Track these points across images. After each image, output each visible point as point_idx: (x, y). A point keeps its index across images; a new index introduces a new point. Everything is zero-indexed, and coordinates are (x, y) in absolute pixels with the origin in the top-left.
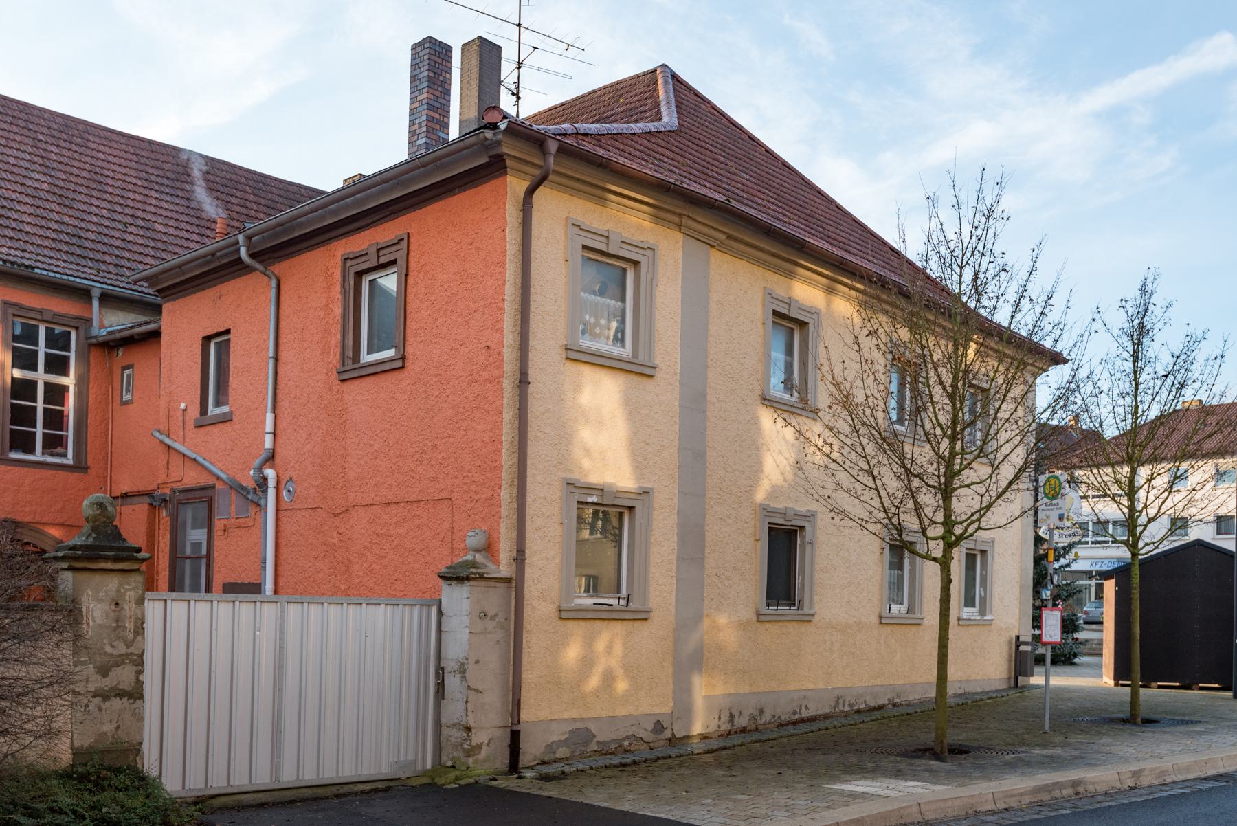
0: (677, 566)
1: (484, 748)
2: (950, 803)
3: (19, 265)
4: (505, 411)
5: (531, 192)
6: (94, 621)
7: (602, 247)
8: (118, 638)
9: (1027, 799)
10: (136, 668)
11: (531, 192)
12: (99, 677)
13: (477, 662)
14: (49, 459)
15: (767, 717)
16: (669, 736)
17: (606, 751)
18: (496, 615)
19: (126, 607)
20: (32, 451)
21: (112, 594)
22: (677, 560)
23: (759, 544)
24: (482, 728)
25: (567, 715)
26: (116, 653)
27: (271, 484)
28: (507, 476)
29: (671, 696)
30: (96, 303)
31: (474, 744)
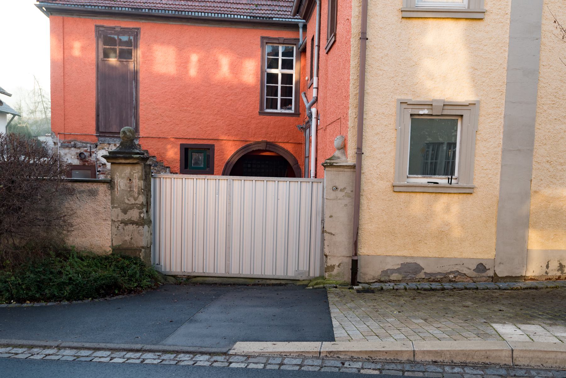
0: (503, 159)
1: (336, 268)
2: (553, 355)
3: (266, 18)
4: (352, 59)
6: (120, 187)
8: (131, 196)
10: (139, 211)
12: (123, 214)
13: (331, 217)
14: (283, 111)
17: (431, 278)
18: (345, 188)
19: (134, 181)
20: (277, 108)
21: (128, 175)
22: (503, 152)
24: (334, 256)
25: (399, 253)
26: (130, 203)
27: (314, 116)
28: (353, 101)
29: (494, 247)
30: (301, 30)
31: (329, 265)
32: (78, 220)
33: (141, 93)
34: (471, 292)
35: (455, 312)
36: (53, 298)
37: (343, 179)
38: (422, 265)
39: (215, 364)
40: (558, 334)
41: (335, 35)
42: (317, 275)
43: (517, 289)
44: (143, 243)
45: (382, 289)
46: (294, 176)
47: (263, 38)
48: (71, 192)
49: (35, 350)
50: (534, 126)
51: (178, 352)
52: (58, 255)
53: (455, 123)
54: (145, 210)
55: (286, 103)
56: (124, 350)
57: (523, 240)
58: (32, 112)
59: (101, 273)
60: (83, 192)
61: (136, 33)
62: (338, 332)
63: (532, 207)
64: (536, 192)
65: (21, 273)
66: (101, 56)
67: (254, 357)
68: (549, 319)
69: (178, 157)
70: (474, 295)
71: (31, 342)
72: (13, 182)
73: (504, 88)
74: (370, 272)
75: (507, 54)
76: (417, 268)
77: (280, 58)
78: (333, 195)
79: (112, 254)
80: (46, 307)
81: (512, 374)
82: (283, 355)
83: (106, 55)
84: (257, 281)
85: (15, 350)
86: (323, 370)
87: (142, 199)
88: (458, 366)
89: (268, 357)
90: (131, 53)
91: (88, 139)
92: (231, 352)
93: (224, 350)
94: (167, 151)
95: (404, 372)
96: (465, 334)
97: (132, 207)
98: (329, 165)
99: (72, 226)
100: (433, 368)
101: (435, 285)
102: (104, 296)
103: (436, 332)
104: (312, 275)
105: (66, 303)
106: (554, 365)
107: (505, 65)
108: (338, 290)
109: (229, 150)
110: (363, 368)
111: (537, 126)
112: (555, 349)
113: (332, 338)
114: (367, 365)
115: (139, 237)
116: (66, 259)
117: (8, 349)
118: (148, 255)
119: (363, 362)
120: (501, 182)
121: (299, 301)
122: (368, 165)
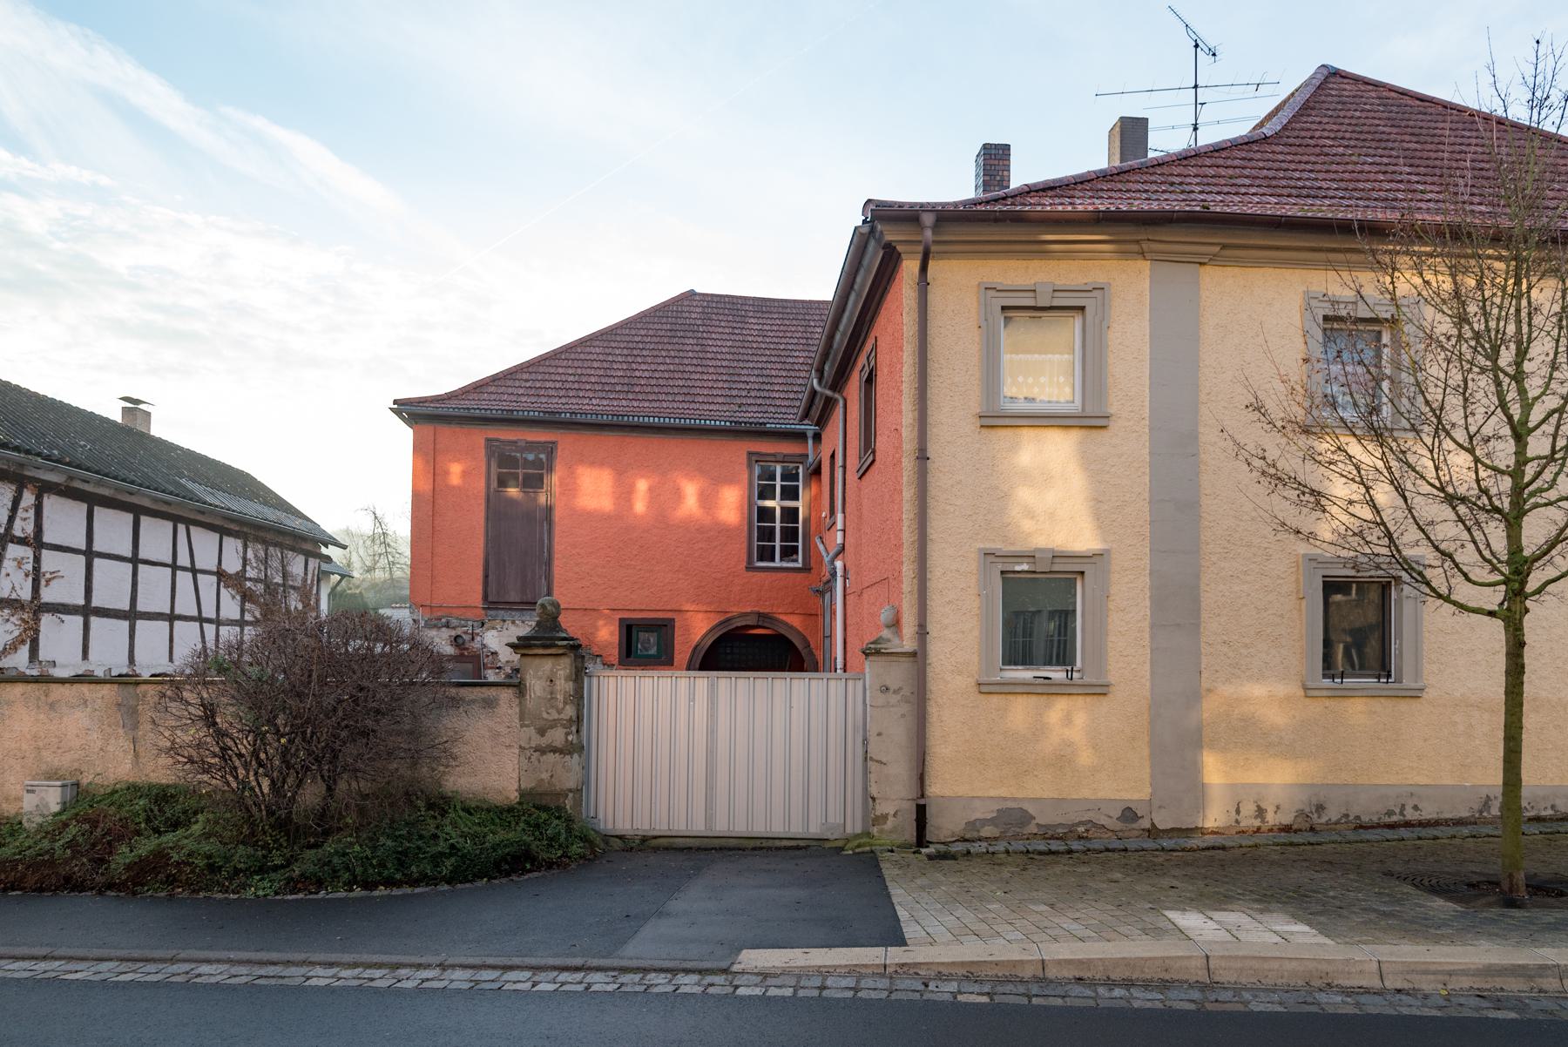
0: (1152, 637)
1: (891, 819)
2: (1275, 965)
5: (924, 268)
7: (1031, 303)
9: (1465, 982)
11: (924, 268)
14: (785, 565)
15: (1333, 814)
16: (1147, 825)
17: (1048, 834)
20: (773, 560)
23: (1304, 603)
25: (993, 793)
27: (839, 573)
28: (908, 553)
29: (1147, 777)
30: (810, 442)
32: (465, 749)
33: (556, 539)
34: (1116, 855)
35: (1097, 891)
36: (423, 879)
37: (897, 674)
38: (1031, 811)
39: (711, 990)
40: (1278, 928)
41: (874, 452)
42: (858, 830)
43: (1191, 850)
44: (572, 784)
45: (969, 852)
46: (801, 669)
47: (750, 453)
48: (455, 702)
49: (403, 972)
50: (1198, 587)
51: (645, 971)
52: (431, 806)
53: (1071, 584)
54: (574, 729)
55: (789, 552)
56: (554, 968)
57: (1195, 769)
58: (370, 570)
59: (502, 835)
60: (474, 701)
61: (550, 449)
62: (909, 931)
63: (1205, 715)
64: (1209, 690)
65: (371, 839)
66: (494, 484)
67: (775, 976)
68: (1256, 901)
69: (615, 639)
70: (1124, 861)
71: (395, 959)
72: (361, 689)
73: (1147, 530)
74: (944, 825)
75: (1147, 479)
76: (1026, 817)
77: (778, 483)
78: (882, 699)
79: (520, 803)
80: (413, 895)
81: (1213, 998)
82: (824, 972)
83: (502, 483)
84: (758, 843)
85: (368, 973)
86: (893, 996)
87: (570, 711)
88: (1119, 986)
89: (800, 974)
90: (541, 478)
91: (469, 614)
92: (735, 968)
93: (724, 965)
94: (597, 629)
95: (1029, 997)
96: (1124, 929)
97: (553, 724)
98: (872, 652)
99: (455, 759)
100: (1077, 990)
101: (1055, 845)
102: (508, 874)
103: (1074, 927)
104: (849, 830)
105: (446, 887)
106: (1279, 982)
107: (1147, 495)
108: (895, 857)
109: (697, 627)
110: (960, 992)
111: (1203, 587)
112: (1278, 954)
113: (901, 941)
114: (967, 987)
115: (565, 773)
116: (444, 813)
117: (357, 971)
118: (578, 803)
119: (960, 981)
120: (1152, 673)
121: (836, 876)
122: (939, 653)
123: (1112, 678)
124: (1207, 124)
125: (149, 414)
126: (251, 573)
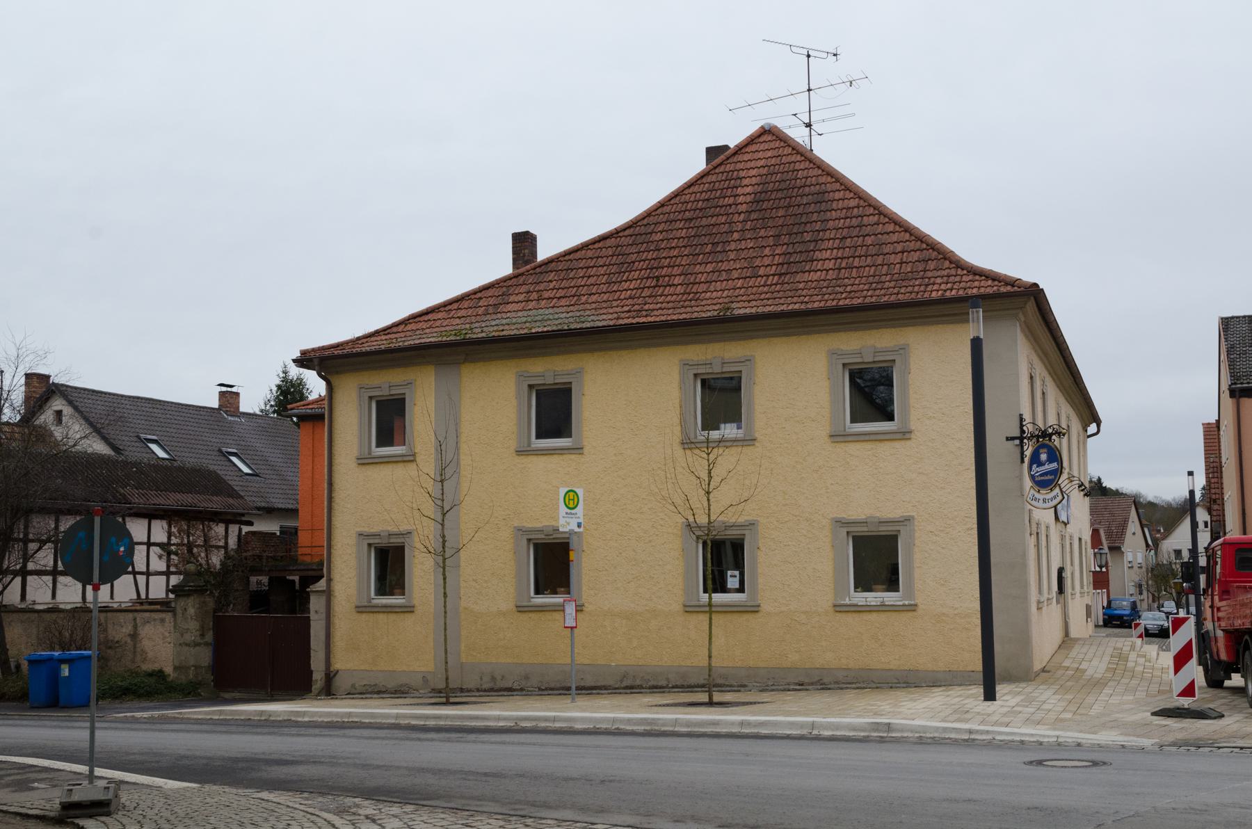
123: (416, 602)
124: (818, 122)
125: (237, 394)
126: (174, 540)
